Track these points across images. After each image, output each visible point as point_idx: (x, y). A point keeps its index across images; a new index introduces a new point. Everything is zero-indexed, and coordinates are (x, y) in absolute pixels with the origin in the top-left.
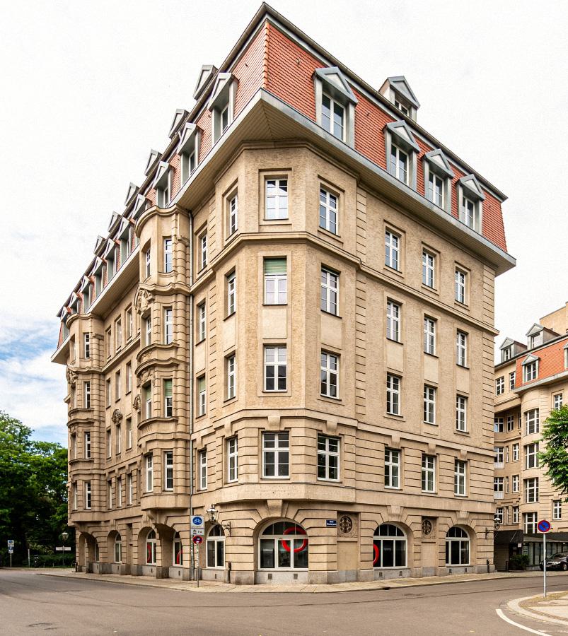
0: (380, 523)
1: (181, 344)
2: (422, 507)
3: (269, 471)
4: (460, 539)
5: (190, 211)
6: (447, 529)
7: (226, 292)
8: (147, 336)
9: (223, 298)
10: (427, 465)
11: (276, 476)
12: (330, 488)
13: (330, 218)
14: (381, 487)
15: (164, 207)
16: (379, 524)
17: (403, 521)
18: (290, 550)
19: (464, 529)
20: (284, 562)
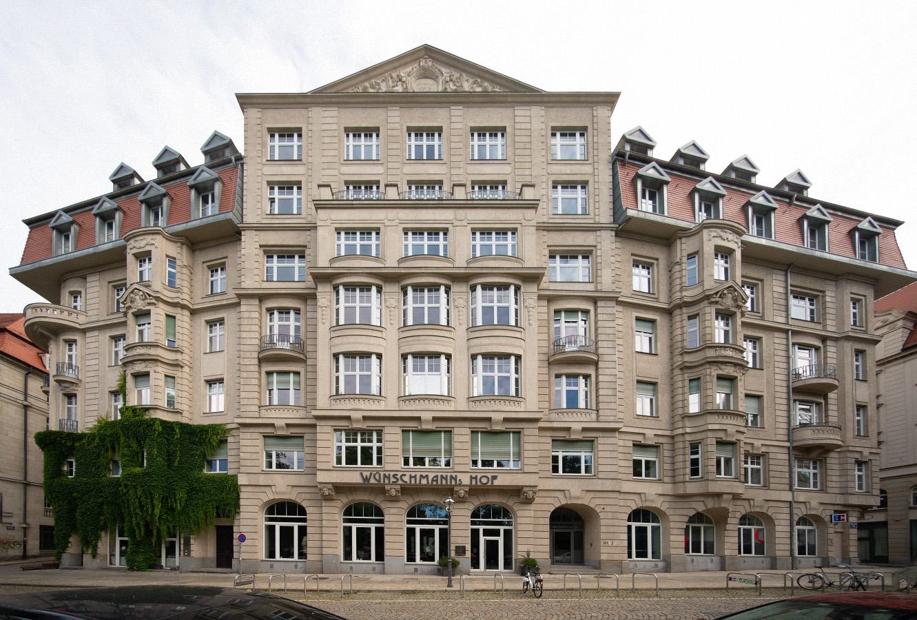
0: (634, 507)
1: (677, 372)
2: (610, 490)
3: (555, 469)
4: (806, 528)
5: (668, 239)
6: (739, 515)
7: (110, 352)
8: (402, 379)
9: (868, 313)
10: (749, 463)
11: (644, 477)
12: (345, 473)
13: (284, 263)
14: (551, 474)
15: (296, 279)
16: (634, 509)
17: (765, 511)
18: (799, 540)
19: (757, 516)
20: (382, 521)
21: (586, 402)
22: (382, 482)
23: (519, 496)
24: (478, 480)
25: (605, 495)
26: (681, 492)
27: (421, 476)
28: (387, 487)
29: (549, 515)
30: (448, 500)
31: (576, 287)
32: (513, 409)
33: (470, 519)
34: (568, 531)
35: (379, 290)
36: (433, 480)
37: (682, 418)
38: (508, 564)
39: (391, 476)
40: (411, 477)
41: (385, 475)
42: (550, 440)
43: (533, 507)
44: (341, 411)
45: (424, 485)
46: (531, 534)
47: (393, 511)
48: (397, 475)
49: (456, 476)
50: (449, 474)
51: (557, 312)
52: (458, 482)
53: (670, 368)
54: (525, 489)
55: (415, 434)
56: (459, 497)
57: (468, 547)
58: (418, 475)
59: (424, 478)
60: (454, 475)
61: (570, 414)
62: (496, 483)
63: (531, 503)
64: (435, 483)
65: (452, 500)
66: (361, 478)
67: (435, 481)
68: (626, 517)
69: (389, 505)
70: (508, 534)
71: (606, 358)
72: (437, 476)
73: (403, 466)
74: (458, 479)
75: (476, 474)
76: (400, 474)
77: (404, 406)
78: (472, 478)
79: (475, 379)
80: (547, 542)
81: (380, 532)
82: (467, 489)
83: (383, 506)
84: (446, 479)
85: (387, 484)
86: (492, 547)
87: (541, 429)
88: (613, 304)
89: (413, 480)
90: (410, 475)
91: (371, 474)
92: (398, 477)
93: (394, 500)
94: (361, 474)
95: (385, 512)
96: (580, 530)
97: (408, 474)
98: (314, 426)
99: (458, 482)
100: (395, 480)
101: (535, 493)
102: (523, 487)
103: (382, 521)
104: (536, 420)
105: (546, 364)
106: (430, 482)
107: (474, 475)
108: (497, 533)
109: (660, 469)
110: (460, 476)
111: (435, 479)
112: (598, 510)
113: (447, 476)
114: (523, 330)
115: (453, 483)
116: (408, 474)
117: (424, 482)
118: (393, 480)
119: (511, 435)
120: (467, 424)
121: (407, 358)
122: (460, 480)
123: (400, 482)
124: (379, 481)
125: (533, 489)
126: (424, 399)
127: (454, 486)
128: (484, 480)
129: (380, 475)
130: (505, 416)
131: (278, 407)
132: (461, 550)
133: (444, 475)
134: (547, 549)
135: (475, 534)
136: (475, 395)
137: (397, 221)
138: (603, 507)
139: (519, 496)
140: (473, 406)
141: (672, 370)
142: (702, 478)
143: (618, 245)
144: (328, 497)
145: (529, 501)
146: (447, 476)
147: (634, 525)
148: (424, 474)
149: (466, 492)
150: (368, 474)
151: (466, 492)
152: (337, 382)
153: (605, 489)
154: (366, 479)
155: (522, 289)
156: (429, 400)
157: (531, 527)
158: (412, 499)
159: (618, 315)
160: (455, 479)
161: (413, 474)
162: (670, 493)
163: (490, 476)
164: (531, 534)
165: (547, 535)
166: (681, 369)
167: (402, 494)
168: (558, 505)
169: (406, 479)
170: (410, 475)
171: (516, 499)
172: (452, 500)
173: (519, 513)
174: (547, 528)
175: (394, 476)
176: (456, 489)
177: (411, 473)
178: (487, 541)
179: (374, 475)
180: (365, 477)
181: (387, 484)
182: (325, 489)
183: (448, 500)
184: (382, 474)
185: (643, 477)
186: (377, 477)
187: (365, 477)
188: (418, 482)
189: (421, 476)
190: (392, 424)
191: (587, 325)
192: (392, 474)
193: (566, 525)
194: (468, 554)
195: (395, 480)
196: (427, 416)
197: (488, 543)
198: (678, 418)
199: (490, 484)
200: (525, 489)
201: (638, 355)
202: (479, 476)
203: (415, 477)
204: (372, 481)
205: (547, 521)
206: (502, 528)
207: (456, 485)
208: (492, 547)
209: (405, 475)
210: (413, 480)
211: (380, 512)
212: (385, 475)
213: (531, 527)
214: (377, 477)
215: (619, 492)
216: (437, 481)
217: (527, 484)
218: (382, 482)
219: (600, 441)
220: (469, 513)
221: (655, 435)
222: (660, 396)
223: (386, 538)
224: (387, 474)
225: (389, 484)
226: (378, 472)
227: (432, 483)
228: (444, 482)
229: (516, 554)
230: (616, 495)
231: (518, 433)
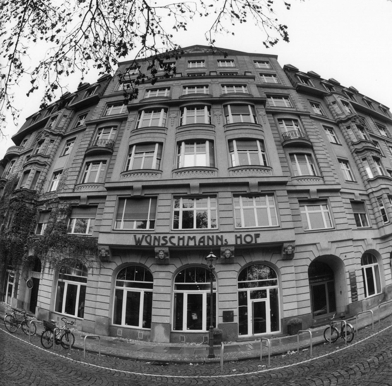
20: (151, 286)
21: (314, 172)
22: (152, 244)
23: (280, 253)
24: (243, 240)
25: (344, 244)
26: (383, 235)
27: (189, 238)
28: (156, 250)
29: (306, 269)
30: (209, 256)
31: (286, 109)
32: (265, 175)
33: (236, 282)
34: (322, 283)
35: (166, 111)
36: (200, 242)
37: (368, 182)
38: (274, 327)
39: (161, 238)
40: (179, 239)
41: (155, 238)
42: (296, 201)
43: (292, 263)
44: (127, 183)
45: (192, 247)
46: (294, 291)
47: (162, 275)
48: (166, 237)
49: (222, 236)
50: (215, 235)
51: (280, 120)
52: (224, 242)
53: (350, 153)
54: (285, 245)
55: (240, 143)
56: (226, 258)
57: (236, 312)
58: (186, 236)
59: (192, 239)
60: (220, 235)
61: (309, 180)
62: (260, 241)
63: (291, 259)
64: (202, 244)
65: (213, 256)
66: (134, 241)
67: (202, 242)
68: (359, 261)
69: (158, 268)
70: (274, 293)
71: (316, 144)
72: (203, 237)
73: (173, 229)
74: (224, 239)
75: (241, 233)
76: (169, 236)
77: (176, 176)
78: (237, 237)
79: (233, 156)
80: (308, 296)
81: (149, 297)
82: (233, 249)
83: (153, 269)
84: (212, 240)
85: (156, 246)
86: (259, 309)
87: (289, 192)
88: (308, 118)
89: (181, 242)
90: (179, 237)
91: (143, 236)
92: (168, 239)
93: (163, 263)
94: (135, 236)
95: (155, 276)
96: (331, 281)
97: (176, 236)
98: (104, 197)
99: (224, 242)
100: (164, 242)
101: (293, 248)
102: (282, 243)
103: (151, 286)
104: (284, 184)
105: (281, 147)
106: (197, 244)
107: (238, 235)
108: (263, 294)
109: (368, 218)
110: (226, 236)
111: (202, 240)
112: (342, 258)
113: (213, 236)
114: (216, 170)
115: (220, 243)
116: (176, 236)
117: (192, 243)
118: (162, 242)
119: (151, 200)
120: (229, 189)
121: (181, 145)
122: (226, 240)
123: (169, 244)
124: (150, 243)
125: (291, 244)
126: (192, 171)
127: (220, 246)
128: (248, 239)
129: (151, 237)
130: (259, 181)
131: (98, 184)
132: (228, 316)
133: (211, 235)
134: (309, 303)
135: (242, 299)
136: (234, 166)
137: (180, 84)
138: (345, 255)
139: (280, 253)
140: (232, 174)
141: (352, 154)
142: (389, 222)
143: (298, 95)
144: (105, 259)
145: (289, 257)
146: (213, 236)
147: (365, 267)
148: (192, 236)
149: (232, 252)
150: (140, 236)
151: (232, 252)
152: (129, 164)
153: (343, 239)
154: (138, 242)
155: (256, 107)
156: (197, 170)
157: (293, 284)
158: (180, 263)
159: (313, 123)
160: (221, 240)
161: (181, 236)
162: (379, 236)
163: (253, 234)
164: (294, 291)
165: (308, 289)
166: (356, 153)
167: (171, 257)
168: (313, 258)
169: (175, 241)
170: (179, 237)
171: (279, 257)
172: (213, 256)
173: (283, 271)
174: (307, 282)
175: (164, 238)
176: (222, 249)
177: (179, 235)
178: (254, 303)
179: (147, 237)
180: (137, 239)
181: (156, 246)
182: (103, 251)
183: (209, 256)
184: (153, 236)
185: (362, 227)
186: (148, 240)
187: (137, 239)
188: (186, 244)
189: (189, 238)
190: (165, 191)
191: (299, 127)
192: (162, 236)
193: (321, 278)
194: (236, 320)
195: (164, 242)
196: (195, 183)
197: (255, 305)
198: (366, 182)
199: (254, 242)
200: (285, 245)
201: (331, 144)
202: (243, 235)
203: (183, 239)
204: (144, 243)
205: (306, 275)
206: (268, 288)
207: (222, 245)
208: (259, 309)
209: (173, 237)
210: (181, 242)
211: (150, 277)
212: (155, 238)
213: (293, 284)
214: (148, 240)
215: (352, 240)
216: (203, 242)
217: (286, 240)
218: (152, 244)
219: (331, 199)
220: (236, 275)
221: (360, 194)
222: (352, 168)
223: (154, 304)
224: (157, 236)
225: (159, 246)
226: (149, 235)
227: (199, 244)
228: (211, 243)
229: (282, 314)
230: (350, 243)
231: (155, 198)
